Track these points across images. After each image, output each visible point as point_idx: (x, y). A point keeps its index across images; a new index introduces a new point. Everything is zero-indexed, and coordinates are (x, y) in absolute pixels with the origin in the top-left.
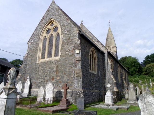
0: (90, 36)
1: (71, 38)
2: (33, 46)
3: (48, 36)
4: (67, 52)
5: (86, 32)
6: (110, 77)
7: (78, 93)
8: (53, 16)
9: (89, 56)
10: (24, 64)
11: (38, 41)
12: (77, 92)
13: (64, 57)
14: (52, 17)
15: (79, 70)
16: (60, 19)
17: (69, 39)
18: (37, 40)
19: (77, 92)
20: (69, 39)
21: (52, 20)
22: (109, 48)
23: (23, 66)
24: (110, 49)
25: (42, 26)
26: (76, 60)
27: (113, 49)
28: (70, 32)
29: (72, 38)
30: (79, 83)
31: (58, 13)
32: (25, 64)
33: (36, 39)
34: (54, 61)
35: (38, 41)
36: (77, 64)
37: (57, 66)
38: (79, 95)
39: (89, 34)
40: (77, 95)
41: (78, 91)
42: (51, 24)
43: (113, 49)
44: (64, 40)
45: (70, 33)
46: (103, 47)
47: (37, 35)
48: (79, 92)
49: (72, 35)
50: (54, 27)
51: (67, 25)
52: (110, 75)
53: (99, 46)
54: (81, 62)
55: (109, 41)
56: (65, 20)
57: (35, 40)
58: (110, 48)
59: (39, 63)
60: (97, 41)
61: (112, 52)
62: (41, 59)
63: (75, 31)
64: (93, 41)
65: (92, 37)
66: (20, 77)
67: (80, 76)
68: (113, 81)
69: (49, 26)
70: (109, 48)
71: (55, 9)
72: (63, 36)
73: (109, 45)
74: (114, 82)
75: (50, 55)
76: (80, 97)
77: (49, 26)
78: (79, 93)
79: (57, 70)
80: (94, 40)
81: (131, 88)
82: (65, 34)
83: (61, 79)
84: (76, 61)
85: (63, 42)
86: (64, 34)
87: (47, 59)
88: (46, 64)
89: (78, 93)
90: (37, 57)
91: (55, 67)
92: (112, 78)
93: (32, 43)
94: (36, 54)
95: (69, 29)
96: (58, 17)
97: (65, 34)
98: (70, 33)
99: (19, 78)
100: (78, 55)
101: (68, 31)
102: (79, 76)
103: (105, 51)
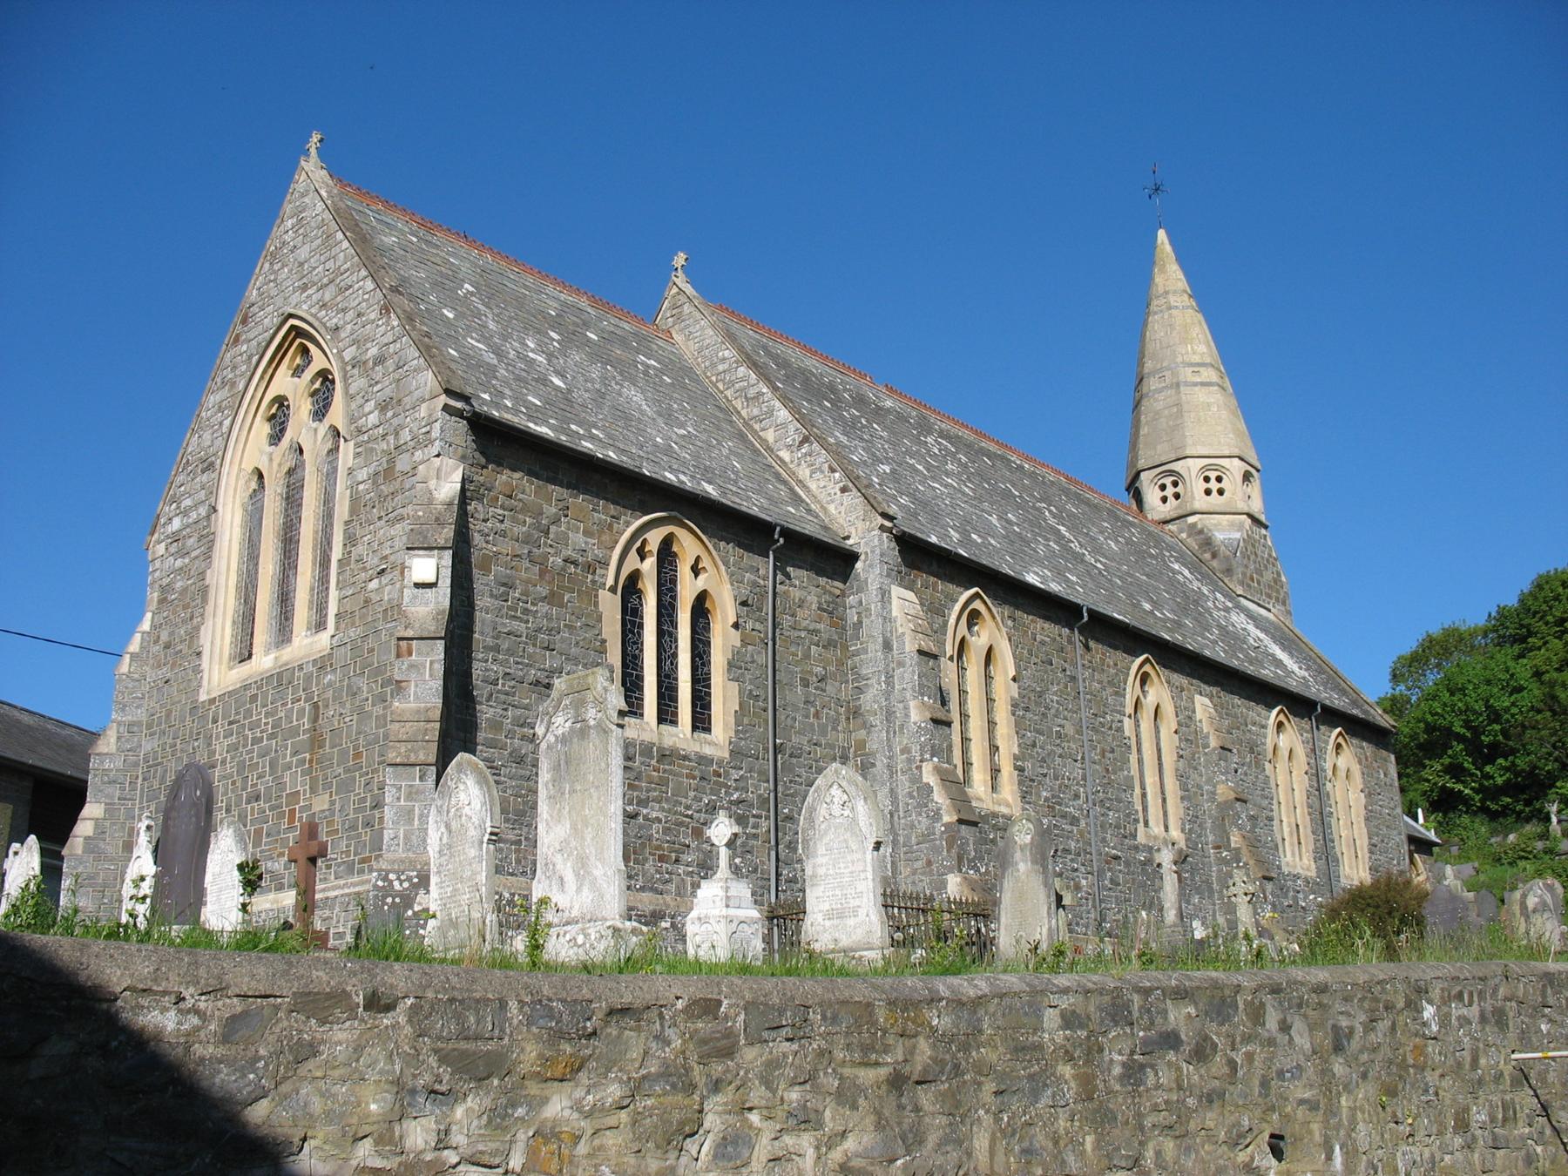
0: (738, 404)
1: (402, 464)
2: (179, 563)
3: (273, 462)
4: (374, 585)
5: (714, 365)
6: (915, 780)
7: (396, 883)
8: (304, 288)
9: (610, 606)
10: (119, 724)
11: (208, 517)
12: (385, 879)
13: (353, 624)
14: (295, 298)
15: (418, 711)
16: (343, 310)
17: (389, 473)
18: (203, 511)
19: (385, 879)
20: (389, 473)
21: (293, 327)
22: (1213, 475)
23: (113, 740)
24: (1221, 492)
25: (234, 384)
26: (399, 639)
27: (1214, 485)
28: (394, 416)
29: (406, 456)
30: (411, 811)
31: (330, 264)
32: (132, 724)
33: (196, 506)
34: (301, 667)
35: (208, 517)
36: (412, 666)
37: (316, 706)
38: (401, 897)
39: (732, 383)
40: (389, 900)
41: (399, 873)
42: (293, 359)
43: (1214, 485)
44: (361, 487)
45: (395, 422)
46: (844, 490)
47: (203, 472)
48: (409, 879)
49: (405, 435)
50: (312, 382)
51: (380, 360)
52: (909, 761)
53: (813, 486)
54: (440, 645)
55: (1159, 406)
56: (373, 316)
57: (194, 515)
58: (1219, 479)
59: (212, 701)
60: (798, 439)
61: (1191, 520)
62: (231, 668)
63: (424, 401)
64: (763, 441)
65: (756, 412)
66: (96, 827)
67: (422, 757)
68: (937, 816)
69: (284, 382)
70: (1213, 475)
71: (319, 228)
72: (357, 455)
73: (1162, 452)
74: (946, 819)
75: (283, 632)
76: (410, 913)
77: (284, 382)
78: (406, 885)
79: (316, 742)
80: (770, 436)
81: (1018, 855)
82: (366, 437)
83: (337, 806)
84: (403, 644)
85: (356, 504)
86: (360, 431)
87: (264, 661)
88: (254, 698)
89: (396, 883)
90: (199, 654)
91: (301, 712)
92: (929, 789)
93: (176, 538)
94: (197, 629)
95: (388, 391)
96: (328, 295)
97: (366, 437)
98: (395, 422)
99: (86, 838)
100: (429, 593)
101: (383, 408)
102: (412, 760)
103: (860, 524)
